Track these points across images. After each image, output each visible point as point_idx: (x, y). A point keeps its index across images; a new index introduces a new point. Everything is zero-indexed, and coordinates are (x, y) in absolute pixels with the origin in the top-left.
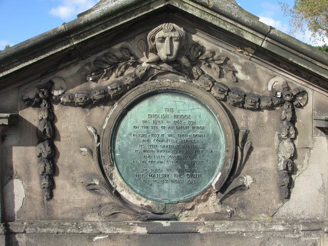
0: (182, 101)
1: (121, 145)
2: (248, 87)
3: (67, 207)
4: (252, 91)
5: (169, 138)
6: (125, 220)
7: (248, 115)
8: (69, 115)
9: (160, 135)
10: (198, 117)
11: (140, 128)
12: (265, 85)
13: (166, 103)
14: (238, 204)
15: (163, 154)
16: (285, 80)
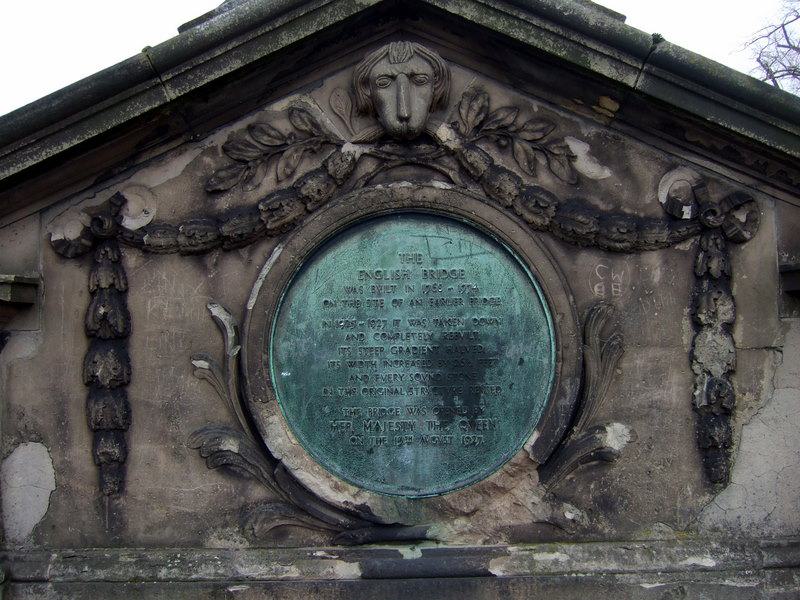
2: (607, 196)
3: (158, 513)
5: (413, 329)
10: (484, 276)
11: (340, 306)
14: (595, 500)
15: (399, 370)
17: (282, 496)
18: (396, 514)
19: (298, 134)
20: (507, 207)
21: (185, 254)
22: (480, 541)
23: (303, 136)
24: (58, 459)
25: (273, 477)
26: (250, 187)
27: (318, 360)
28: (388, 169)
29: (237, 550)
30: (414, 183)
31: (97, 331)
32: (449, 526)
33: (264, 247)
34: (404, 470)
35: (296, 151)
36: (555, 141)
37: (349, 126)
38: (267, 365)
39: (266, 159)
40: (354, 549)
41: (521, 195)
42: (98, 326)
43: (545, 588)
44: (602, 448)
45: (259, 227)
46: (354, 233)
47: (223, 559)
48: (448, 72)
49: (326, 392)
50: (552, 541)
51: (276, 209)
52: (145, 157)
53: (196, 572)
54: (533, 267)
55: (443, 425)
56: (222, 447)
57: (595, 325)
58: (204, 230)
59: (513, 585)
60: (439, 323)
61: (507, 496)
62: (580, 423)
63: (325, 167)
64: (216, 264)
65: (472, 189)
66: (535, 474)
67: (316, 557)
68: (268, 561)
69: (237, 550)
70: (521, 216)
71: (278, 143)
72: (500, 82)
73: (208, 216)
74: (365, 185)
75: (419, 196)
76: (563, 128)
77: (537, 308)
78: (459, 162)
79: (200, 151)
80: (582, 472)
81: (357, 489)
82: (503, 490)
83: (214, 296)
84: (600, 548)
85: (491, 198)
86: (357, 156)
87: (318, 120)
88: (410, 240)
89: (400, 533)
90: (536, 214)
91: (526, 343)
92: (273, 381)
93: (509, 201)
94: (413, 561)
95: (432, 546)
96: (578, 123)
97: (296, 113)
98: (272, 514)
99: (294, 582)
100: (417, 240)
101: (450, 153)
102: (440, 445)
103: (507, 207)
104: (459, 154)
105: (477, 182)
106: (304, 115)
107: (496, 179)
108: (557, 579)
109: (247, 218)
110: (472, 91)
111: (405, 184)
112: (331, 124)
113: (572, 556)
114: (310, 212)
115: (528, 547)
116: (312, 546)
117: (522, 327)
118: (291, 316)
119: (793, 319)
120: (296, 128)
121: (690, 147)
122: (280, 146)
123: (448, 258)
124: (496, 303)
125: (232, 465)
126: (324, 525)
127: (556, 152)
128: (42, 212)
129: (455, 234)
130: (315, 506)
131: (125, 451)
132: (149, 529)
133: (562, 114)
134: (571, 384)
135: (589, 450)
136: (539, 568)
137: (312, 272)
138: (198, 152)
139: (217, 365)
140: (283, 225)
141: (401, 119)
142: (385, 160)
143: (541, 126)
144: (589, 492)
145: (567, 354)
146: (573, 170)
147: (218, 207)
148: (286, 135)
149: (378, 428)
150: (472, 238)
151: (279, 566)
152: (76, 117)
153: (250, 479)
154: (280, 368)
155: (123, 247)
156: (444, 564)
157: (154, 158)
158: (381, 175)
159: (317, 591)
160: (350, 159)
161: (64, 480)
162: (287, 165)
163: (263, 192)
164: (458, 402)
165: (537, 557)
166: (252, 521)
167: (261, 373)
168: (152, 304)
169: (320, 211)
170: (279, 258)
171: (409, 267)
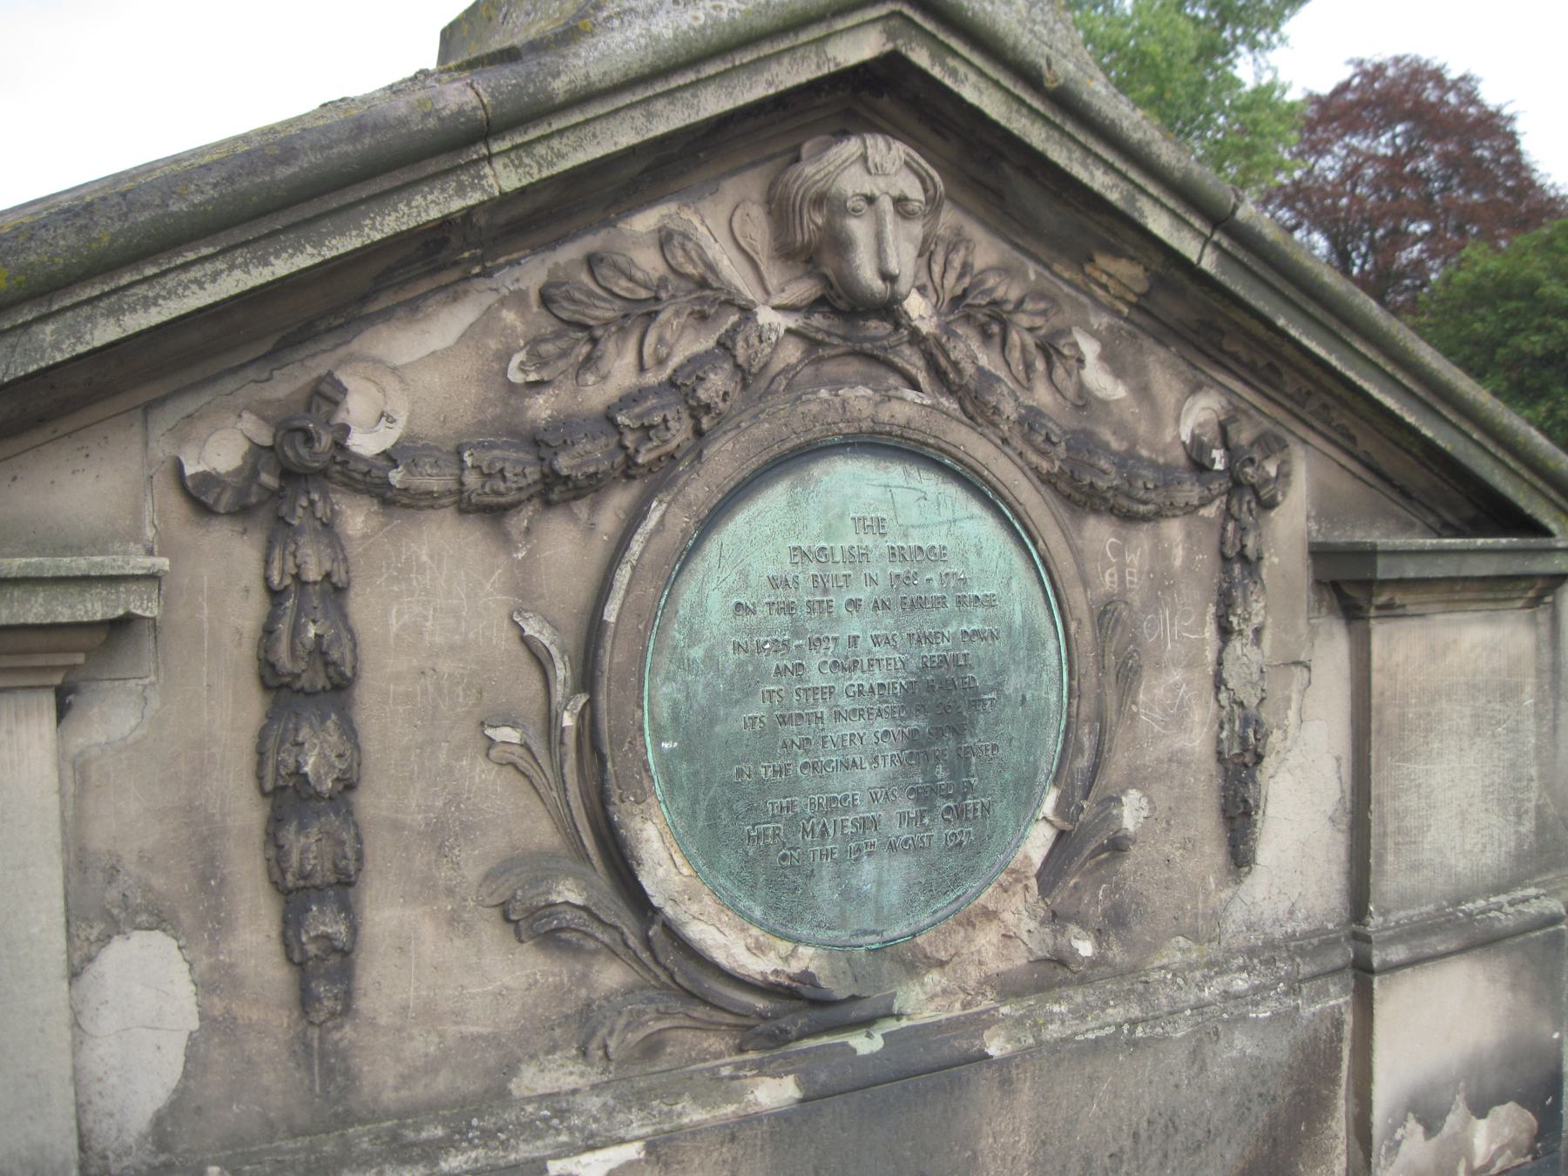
0: (913, 484)
1: (680, 697)
2: (1121, 429)
3: (422, 1044)
4: (1133, 444)
5: (880, 652)
6: (695, 1061)
7: (1125, 540)
8: (425, 558)
9: (844, 640)
10: (972, 557)
11: (763, 611)
12: (1171, 421)
13: (858, 497)
14: (1104, 915)
15: (857, 726)
16: (1230, 403)
17: (656, 977)
21: (466, 506)
22: (958, 1005)
24: (204, 962)
25: (647, 942)
26: (591, 379)
31: (298, 676)
35: (677, 314)
40: (777, 1052)
42: (303, 665)
49: (740, 773)
52: (374, 307)
54: (1041, 543)
61: (994, 925)
63: (725, 346)
64: (528, 531)
71: (643, 294)
75: (884, 415)
80: (1090, 871)
81: (790, 946)
82: (990, 915)
83: (524, 594)
89: (856, 1012)
91: (1030, 669)
94: (872, 1056)
96: (1085, 307)
98: (641, 1013)
99: (696, 1131)
101: (916, 337)
112: (733, 271)
116: (705, 1060)
118: (677, 634)
119: (1321, 620)
121: (1225, 360)
122: (646, 300)
124: (989, 602)
126: (730, 1019)
128: (148, 408)
129: (930, 483)
131: (354, 929)
132: (405, 1080)
134: (1090, 733)
137: (712, 548)
138: (490, 299)
140: (659, 459)
143: (1042, 305)
149: (824, 832)
150: (953, 491)
152: (308, 211)
153: (594, 953)
155: (334, 491)
157: (399, 304)
159: (733, 1139)
161: (218, 1006)
166: (604, 1031)
168: (400, 614)
171: (868, 541)
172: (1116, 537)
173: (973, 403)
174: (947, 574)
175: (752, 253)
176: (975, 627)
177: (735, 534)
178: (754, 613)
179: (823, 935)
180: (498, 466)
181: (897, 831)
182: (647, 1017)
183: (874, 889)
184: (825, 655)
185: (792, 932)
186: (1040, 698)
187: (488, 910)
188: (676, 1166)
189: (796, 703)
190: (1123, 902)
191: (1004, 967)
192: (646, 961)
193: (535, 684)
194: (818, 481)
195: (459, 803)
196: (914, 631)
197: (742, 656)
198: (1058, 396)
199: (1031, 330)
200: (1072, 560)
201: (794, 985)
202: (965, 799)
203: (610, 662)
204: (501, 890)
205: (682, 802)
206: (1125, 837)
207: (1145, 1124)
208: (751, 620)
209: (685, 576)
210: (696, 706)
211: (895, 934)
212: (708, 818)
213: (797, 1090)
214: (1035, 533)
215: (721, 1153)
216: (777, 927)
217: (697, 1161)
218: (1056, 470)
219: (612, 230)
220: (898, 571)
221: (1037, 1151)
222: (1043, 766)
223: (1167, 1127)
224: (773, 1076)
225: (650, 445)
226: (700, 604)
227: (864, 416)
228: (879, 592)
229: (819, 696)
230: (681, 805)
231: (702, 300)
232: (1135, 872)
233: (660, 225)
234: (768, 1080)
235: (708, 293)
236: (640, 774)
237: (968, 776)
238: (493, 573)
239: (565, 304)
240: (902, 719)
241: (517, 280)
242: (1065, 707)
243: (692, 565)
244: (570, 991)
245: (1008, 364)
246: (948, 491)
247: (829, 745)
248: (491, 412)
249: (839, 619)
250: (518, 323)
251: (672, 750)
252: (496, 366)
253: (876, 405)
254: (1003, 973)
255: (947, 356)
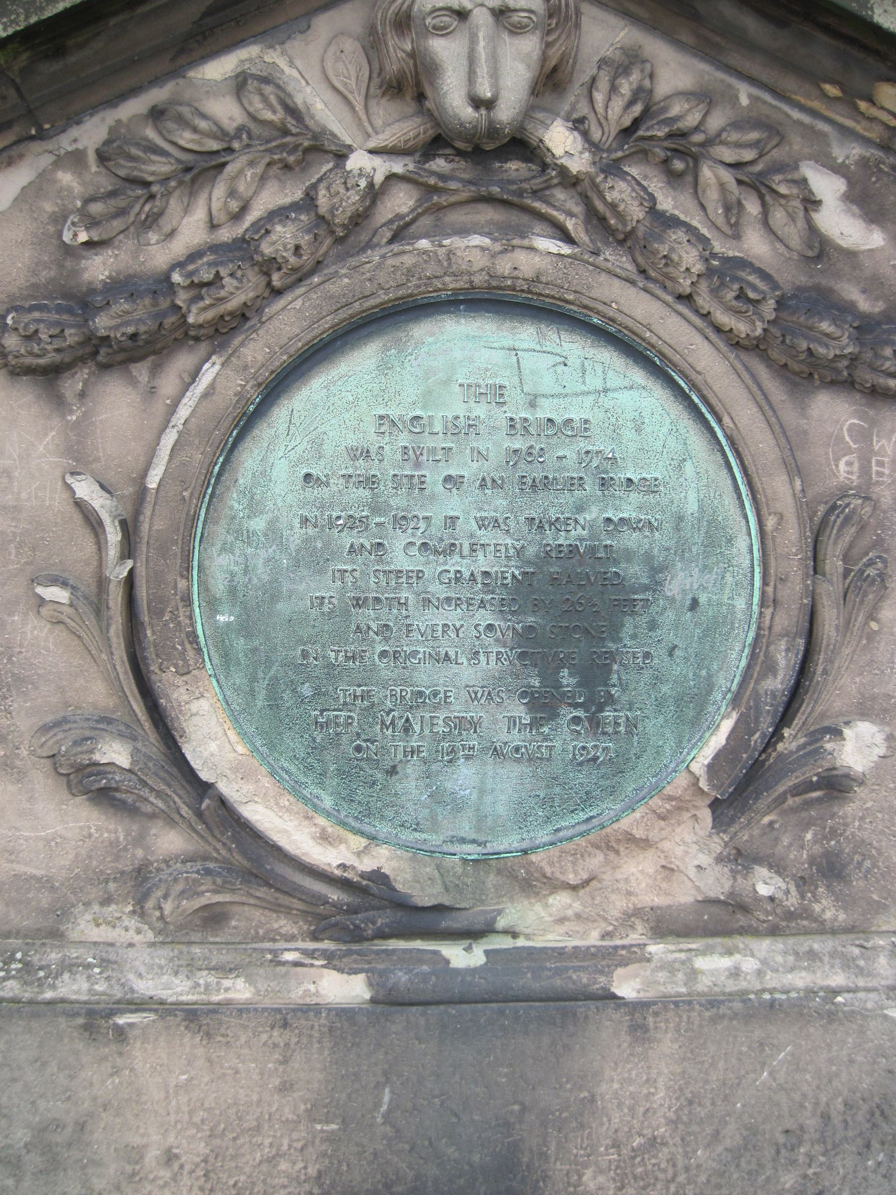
5: (485, 536)
6: (263, 939)
10: (628, 434)
11: (337, 484)
14: (812, 861)
15: (453, 616)
17: (216, 850)
18: (438, 888)
19: (252, 126)
20: (680, 297)
23: (266, 133)
25: (199, 814)
26: (153, 237)
27: (291, 592)
28: (440, 208)
29: (131, 945)
30: (495, 240)
32: (538, 907)
33: (183, 361)
34: (458, 806)
35: (252, 164)
36: (780, 168)
37: (364, 117)
38: (187, 600)
39: (188, 177)
40: (355, 947)
41: (710, 272)
43: (714, 1020)
44: (835, 769)
45: (170, 321)
46: (369, 336)
47: (105, 963)
48: (578, 13)
49: (305, 655)
50: (727, 932)
51: (208, 284)
53: (53, 987)
54: (726, 420)
55: (535, 724)
56: (98, 757)
57: (838, 536)
58: (58, 323)
59: (656, 1014)
60: (537, 525)
61: (650, 854)
62: (797, 722)
63: (309, 201)
64: (82, 395)
65: (612, 257)
66: (706, 815)
67: (284, 963)
68: (192, 967)
69: (131, 945)
70: (706, 316)
71: (214, 145)
72: (670, 37)
73: (66, 296)
74: (391, 241)
75: (504, 266)
76: (797, 143)
77: (729, 500)
78: (586, 200)
79: (50, 158)
80: (794, 810)
81: (364, 842)
82: (645, 844)
84: (816, 946)
85: (648, 278)
86: (379, 178)
87: (299, 100)
88: (484, 357)
90: (737, 312)
92: (200, 632)
93: (685, 285)
94: (473, 971)
95: (504, 943)
96: (825, 135)
97: (252, 85)
99: (242, 1010)
100: (498, 357)
101: (570, 181)
102: (530, 760)
103: (680, 297)
104: (587, 183)
105: (621, 242)
106: (268, 89)
107: (660, 239)
108: (738, 1006)
109: (147, 301)
110: (618, 56)
111: (477, 240)
113: (764, 962)
114: (277, 293)
115: (682, 946)
116: (274, 940)
117: (699, 538)
118: (235, 502)
120: (253, 117)
123: (559, 396)
124: (650, 487)
125: (117, 790)
127: (783, 189)
130: (282, 870)
133: (796, 114)
134: (788, 650)
135: (812, 773)
136: (703, 984)
137: (280, 414)
138: (46, 161)
139: (86, 598)
140: (222, 317)
141: (477, 103)
142: (434, 190)
143: (754, 135)
144: (802, 847)
145: (785, 593)
146: (812, 229)
147: (86, 276)
148: (232, 133)
151: (212, 979)
153: (153, 816)
154: (212, 605)
156: (527, 981)
158: (426, 221)
159: (285, 1025)
160: (363, 183)
162: (232, 193)
163: (179, 247)
164: (567, 679)
165: (700, 963)
166: (159, 893)
167: (175, 618)
169: (301, 290)
170: (212, 386)
171: (480, 411)
172: (860, 418)
173: (642, 254)
174: (587, 452)
175: (346, 93)
176: (625, 515)
177: (309, 400)
178: (327, 484)
179: (407, 836)
180: (32, 328)
181: (504, 736)
182: (203, 888)
183: (474, 797)
184: (413, 535)
185: (367, 829)
186: (720, 604)
187: (42, 761)
188: (219, 1038)
189: (373, 585)
190: (841, 851)
191: (658, 901)
192: (202, 832)
193: (89, 546)
194: (420, 343)
195: (12, 656)
196: (535, 515)
197: (311, 531)
198: (778, 245)
199: (736, 166)
200: (772, 442)
201: (365, 883)
202: (602, 711)
203: (150, 528)
204: (50, 743)
205: (239, 679)
206: (847, 776)
207: (841, 1107)
208: (325, 492)
209: (248, 443)
210: (255, 581)
211: (501, 848)
212: (269, 698)
213: (365, 988)
214: (719, 408)
215: (271, 1037)
216: (350, 820)
217: (243, 1039)
218: (759, 332)
219: (181, 81)
220: (517, 446)
221: (680, 1108)
222: (721, 681)
223: (872, 1114)
224: (340, 970)
225: (201, 304)
226: (263, 474)
227: (475, 268)
228: (488, 468)
229: (404, 580)
230: (238, 681)
231: (282, 147)
232: (862, 819)
233: (239, 70)
234: (334, 973)
235: (288, 139)
236: (182, 644)
237: (606, 685)
238: (46, 434)
239: (122, 162)
240: (513, 613)
241: (75, 141)
242: (755, 616)
243: (256, 432)
244: (125, 849)
245: (703, 207)
246: (599, 357)
247: (416, 635)
248: (45, 275)
249: (433, 497)
250: (75, 184)
251: (228, 624)
252: (51, 229)
253: (493, 256)
254: (659, 908)
255: (602, 198)
